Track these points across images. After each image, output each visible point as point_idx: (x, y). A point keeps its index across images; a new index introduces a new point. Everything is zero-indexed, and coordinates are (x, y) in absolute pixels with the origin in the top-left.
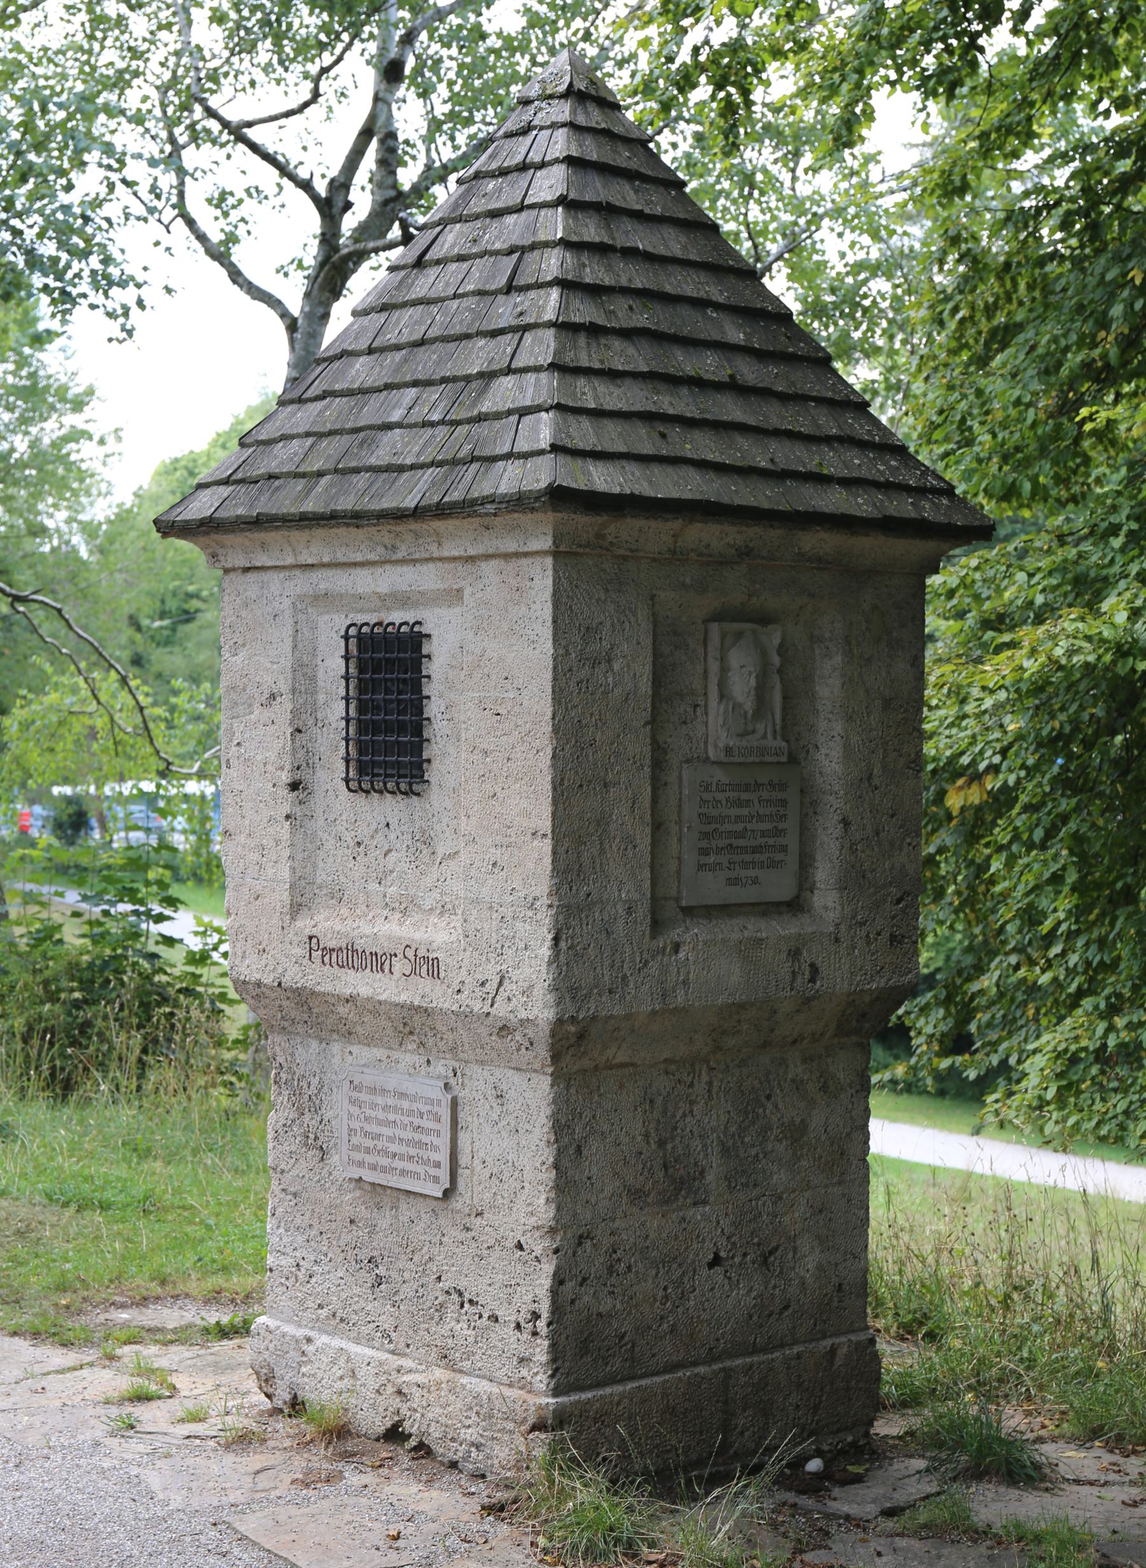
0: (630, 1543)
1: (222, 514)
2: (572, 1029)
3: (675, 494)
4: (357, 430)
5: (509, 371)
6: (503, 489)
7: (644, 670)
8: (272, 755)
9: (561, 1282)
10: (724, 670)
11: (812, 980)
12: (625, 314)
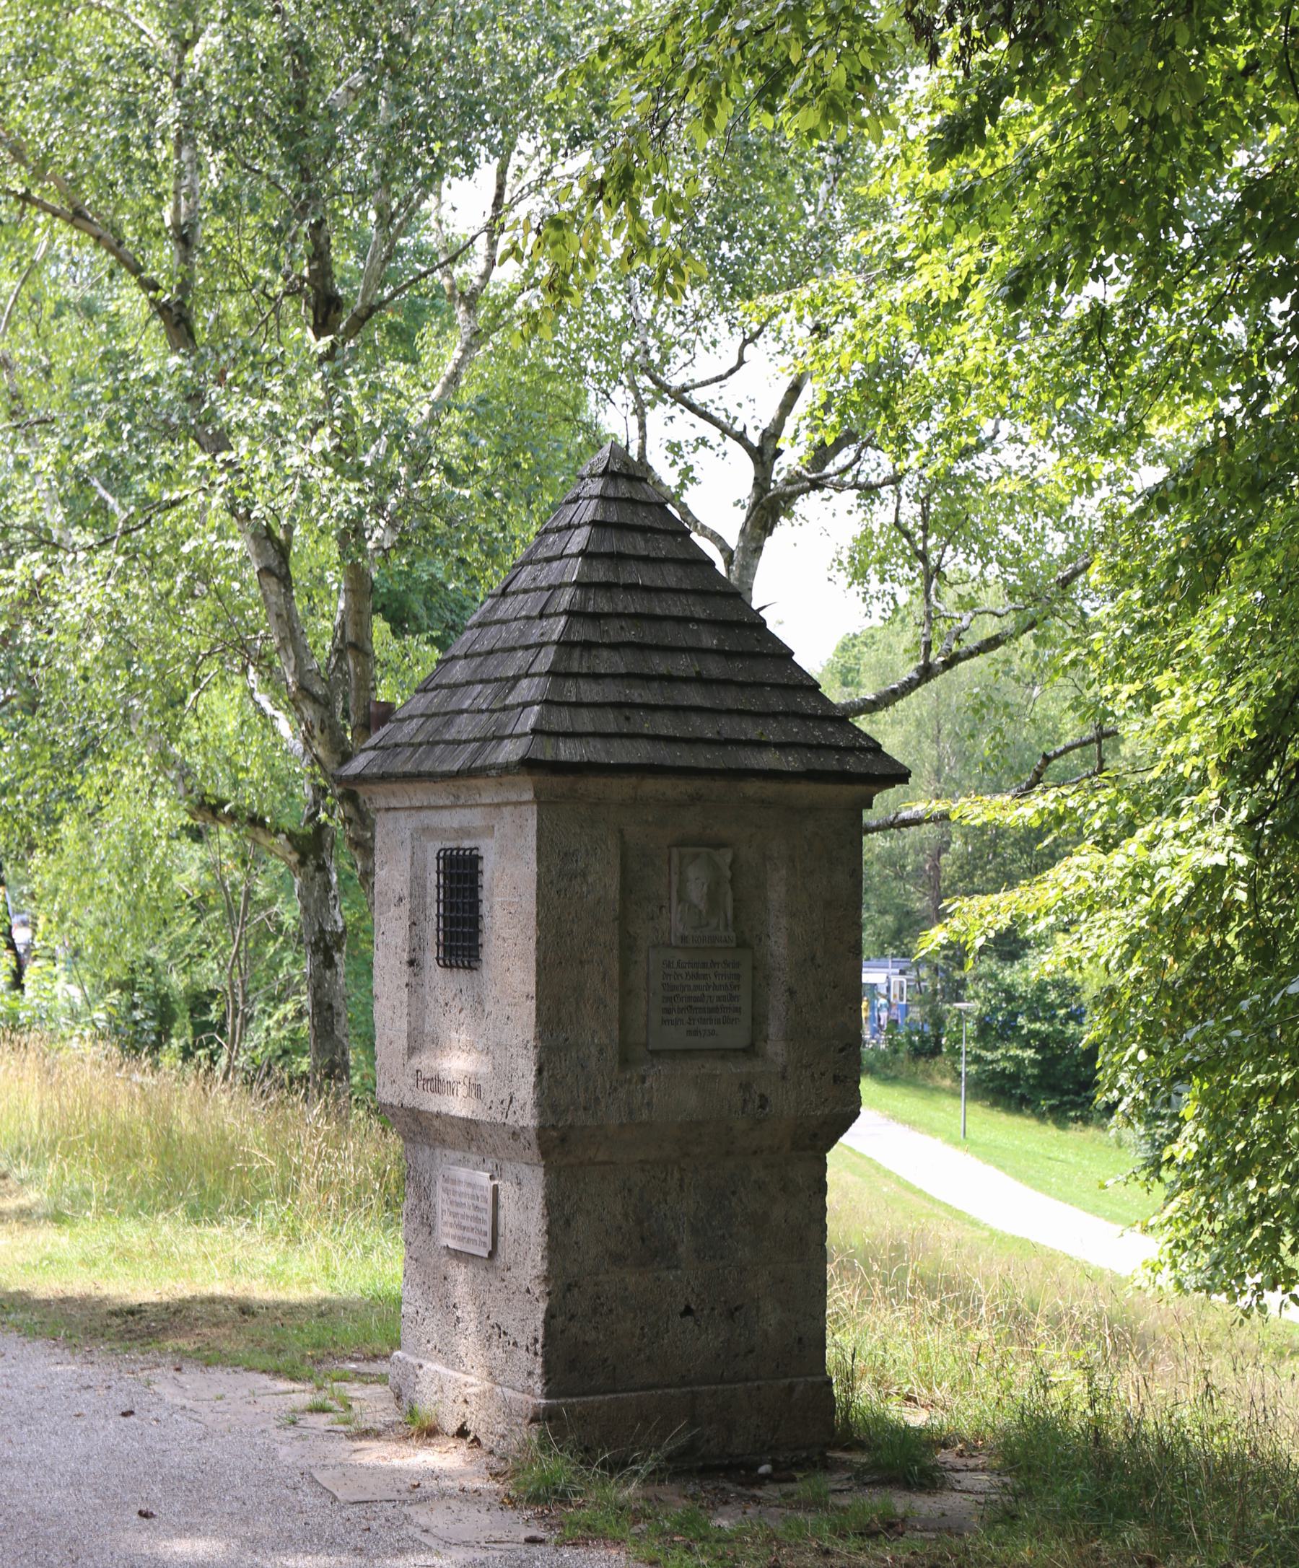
0: (564, 1494)
1: (367, 771)
2: (555, 1134)
3: (626, 760)
4: (446, 714)
5: (527, 675)
6: (500, 760)
7: (613, 882)
8: (399, 941)
9: (553, 1317)
10: (683, 882)
11: (762, 1107)
12: (614, 632)
